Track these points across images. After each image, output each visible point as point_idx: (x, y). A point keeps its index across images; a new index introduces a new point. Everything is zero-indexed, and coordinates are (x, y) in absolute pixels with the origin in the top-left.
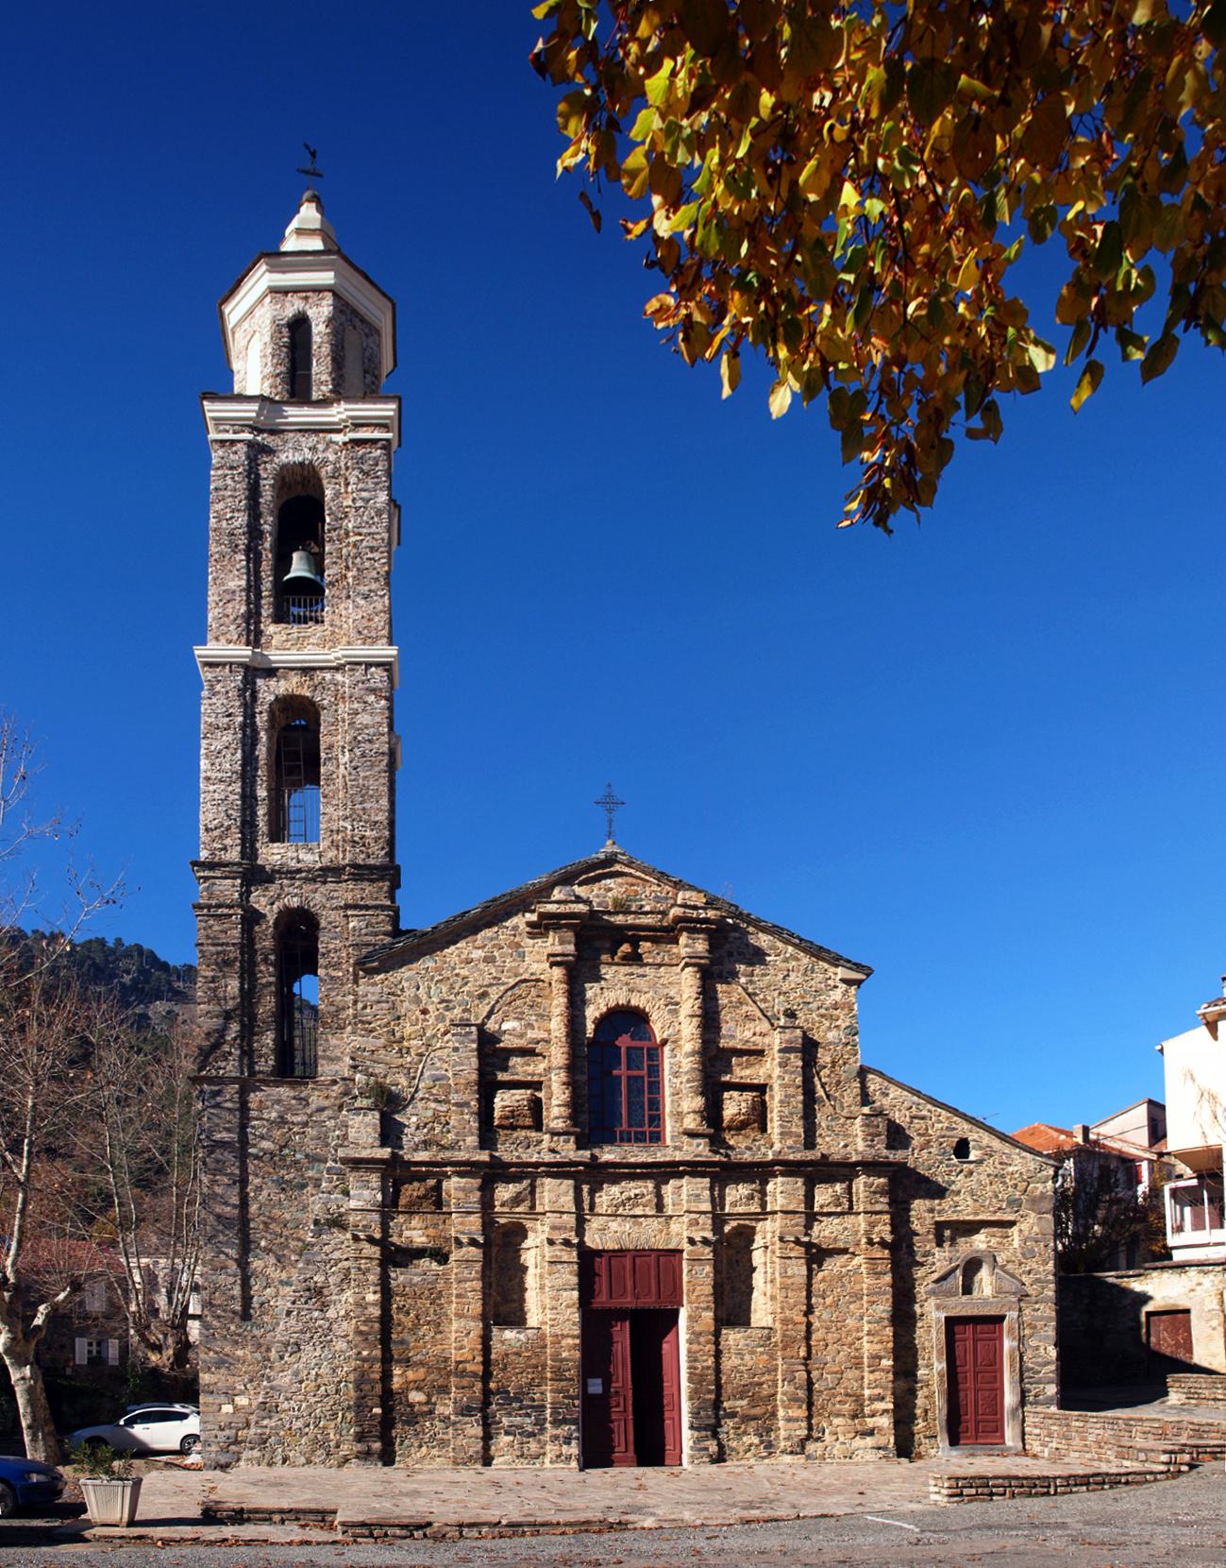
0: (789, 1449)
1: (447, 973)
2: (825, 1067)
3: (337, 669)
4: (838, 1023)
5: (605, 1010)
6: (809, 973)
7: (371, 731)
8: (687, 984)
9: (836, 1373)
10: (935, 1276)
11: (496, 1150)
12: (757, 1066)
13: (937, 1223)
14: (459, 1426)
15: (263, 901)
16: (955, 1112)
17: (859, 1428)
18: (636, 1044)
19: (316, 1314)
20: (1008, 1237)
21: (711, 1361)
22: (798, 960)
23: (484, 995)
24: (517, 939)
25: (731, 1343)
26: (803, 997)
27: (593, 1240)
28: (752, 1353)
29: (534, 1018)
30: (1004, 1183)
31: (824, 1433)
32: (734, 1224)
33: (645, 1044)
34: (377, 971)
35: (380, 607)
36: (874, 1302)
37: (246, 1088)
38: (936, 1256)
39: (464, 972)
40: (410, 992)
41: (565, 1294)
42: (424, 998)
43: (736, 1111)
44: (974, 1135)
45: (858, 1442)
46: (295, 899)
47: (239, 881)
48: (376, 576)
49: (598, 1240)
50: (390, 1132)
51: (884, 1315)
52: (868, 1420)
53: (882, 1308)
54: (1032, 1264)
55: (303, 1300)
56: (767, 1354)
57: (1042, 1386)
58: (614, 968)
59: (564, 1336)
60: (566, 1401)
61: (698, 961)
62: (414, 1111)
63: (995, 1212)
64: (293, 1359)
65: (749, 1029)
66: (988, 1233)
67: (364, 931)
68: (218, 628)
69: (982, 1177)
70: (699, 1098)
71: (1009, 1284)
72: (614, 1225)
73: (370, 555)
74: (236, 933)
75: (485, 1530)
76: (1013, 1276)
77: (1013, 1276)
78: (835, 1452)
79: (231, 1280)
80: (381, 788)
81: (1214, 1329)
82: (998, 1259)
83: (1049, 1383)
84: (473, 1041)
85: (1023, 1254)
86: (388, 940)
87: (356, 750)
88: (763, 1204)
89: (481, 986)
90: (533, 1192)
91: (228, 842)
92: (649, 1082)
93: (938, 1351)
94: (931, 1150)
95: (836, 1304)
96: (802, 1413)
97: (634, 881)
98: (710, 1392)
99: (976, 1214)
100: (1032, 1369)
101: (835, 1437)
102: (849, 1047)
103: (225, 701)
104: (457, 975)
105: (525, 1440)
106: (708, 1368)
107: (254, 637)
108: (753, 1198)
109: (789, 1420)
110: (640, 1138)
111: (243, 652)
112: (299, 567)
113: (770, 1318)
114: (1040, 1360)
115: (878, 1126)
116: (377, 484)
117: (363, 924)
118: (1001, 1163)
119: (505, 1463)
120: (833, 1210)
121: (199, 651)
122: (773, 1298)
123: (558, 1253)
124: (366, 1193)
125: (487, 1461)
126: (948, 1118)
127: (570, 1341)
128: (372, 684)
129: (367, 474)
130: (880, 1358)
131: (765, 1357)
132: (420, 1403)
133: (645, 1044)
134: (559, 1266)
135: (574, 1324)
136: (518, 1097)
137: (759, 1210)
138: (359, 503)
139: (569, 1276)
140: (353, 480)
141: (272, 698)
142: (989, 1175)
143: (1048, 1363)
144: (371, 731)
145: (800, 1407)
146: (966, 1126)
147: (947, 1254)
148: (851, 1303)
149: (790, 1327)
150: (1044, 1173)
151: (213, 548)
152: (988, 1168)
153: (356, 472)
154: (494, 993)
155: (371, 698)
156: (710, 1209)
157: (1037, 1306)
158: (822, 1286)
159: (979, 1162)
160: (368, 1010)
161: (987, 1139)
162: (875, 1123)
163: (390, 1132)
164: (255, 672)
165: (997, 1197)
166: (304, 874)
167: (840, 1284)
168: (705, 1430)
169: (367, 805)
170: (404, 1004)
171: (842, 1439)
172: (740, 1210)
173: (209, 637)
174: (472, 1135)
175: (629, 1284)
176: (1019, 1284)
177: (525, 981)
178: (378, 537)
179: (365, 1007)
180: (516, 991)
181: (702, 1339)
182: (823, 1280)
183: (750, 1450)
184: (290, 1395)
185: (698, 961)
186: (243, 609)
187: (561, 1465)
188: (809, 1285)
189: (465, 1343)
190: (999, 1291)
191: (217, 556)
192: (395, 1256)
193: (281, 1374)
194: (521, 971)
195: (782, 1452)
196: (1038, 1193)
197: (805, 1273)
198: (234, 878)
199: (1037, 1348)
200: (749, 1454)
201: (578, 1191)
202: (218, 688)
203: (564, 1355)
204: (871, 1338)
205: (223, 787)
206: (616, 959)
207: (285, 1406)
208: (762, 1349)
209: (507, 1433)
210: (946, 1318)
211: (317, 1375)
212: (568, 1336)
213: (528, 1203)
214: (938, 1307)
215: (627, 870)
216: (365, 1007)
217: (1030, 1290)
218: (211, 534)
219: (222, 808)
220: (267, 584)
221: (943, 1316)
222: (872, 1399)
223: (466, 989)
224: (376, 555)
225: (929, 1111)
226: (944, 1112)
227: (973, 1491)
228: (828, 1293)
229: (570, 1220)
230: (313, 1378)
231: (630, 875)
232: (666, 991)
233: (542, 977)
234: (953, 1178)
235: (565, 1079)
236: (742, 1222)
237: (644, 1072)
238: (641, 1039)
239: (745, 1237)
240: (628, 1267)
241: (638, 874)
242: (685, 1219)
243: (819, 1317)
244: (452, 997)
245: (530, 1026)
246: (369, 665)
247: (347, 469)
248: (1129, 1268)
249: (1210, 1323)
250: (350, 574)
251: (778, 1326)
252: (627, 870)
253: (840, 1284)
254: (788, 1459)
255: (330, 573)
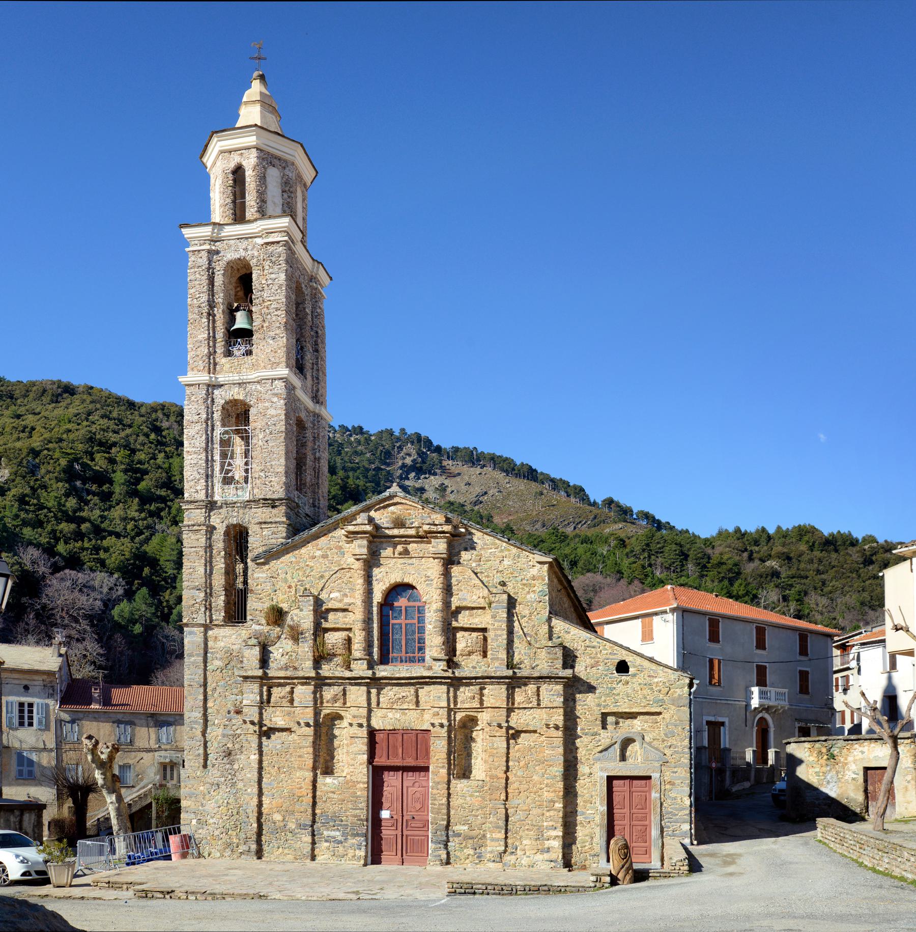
0: (493, 859)
1: (302, 565)
2: (525, 616)
3: (258, 382)
4: (534, 589)
5: (388, 585)
6: (516, 558)
7: (275, 419)
8: (434, 569)
9: (526, 810)
10: (600, 748)
11: (321, 668)
12: (483, 616)
13: (602, 713)
14: (298, 836)
15: (218, 521)
16: (615, 644)
17: (540, 847)
18: (411, 604)
19: (228, 766)
20: (657, 723)
21: (444, 801)
22: (509, 550)
23: (322, 577)
24: (341, 544)
25: (458, 789)
26: (512, 574)
27: (376, 723)
28: (471, 796)
29: (348, 590)
30: (652, 689)
31: (516, 850)
32: (463, 714)
33: (417, 604)
34: (264, 564)
35: (281, 344)
36: (551, 765)
37: (207, 628)
38: (602, 735)
39: (311, 564)
40: (282, 576)
41: (359, 757)
42: (290, 579)
43: (465, 645)
44: (630, 659)
45: (539, 857)
46: (235, 519)
47: (204, 510)
48: (278, 325)
49: (381, 724)
50: (264, 662)
51: (557, 774)
52: (546, 842)
53: (556, 769)
54: (672, 741)
55: (221, 758)
56: (481, 797)
57: (679, 824)
58: (394, 560)
59: (358, 783)
60: (359, 822)
61: (439, 555)
62: (281, 646)
63: (645, 706)
64: (215, 794)
65: (476, 595)
66: (642, 720)
67: (270, 537)
68: (193, 364)
69: (635, 686)
70: (440, 637)
71: (654, 754)
72: (390, 715)
73: (276, 313)
74: (203, 540)
75: (198, 896)
76: (657, 749)
77: (657, 749)
78: (523, 862)
79: (199, 743)
80: (281, 452)
81: (909, 782)
82: (646, 737)
83: (684, 822)
84: (311, 605)
85: (666, 735)
86: (284, 540)
87: (267, 431)
88: (481, 702)
89: (320, 572)
90: (344, 694)
91: (199, 488)
92: (418, 627)
93: (601, 799)
94: (600, 667)
95: (527, 765)
96: (502, 835)
97: (409, 507)
98: (443, 820)
99: (630, 708)
100: (671, 812)
101: (524, 852)
102: (541, 603)
103: (196, 406)
104: (307, 565)
105: (336, 845)
106: (442, 804)
107: (212, 366)
108: (474, 699)
109: (493, 840)
110: (411, 660)
111: (204, 378)
112: (241, 322)
113: (484, 774)
114: (677, 806)
115: (556, 654)
116: (280, 269)
117: (270, 533)
118: (649, 676)
119: (325, 859)
120: (527, 706)
121: (182, 379)
122: (486, 762)
123: (356, 732)
124: (251, 695)
125: (313, 858)
126: (611, 647)
127: (362, 786)
128: (276, 391)
129: (274, 263)
130: (554, 802)
131: (480, 799)
132: (279, 821)
133: (417, 604)
134: (356, 740)
135: (364, 775)
136: (336, 637)
137: (479, 706)
138: (270, 282)
139: (362, 746)
140: (267, 267)
141: (223, 402)
142: (640, 684)
143: (684, 809)
144: (275, 419)
145: (500, 832)
146: (624, 652)
147: (609, 734)
148: (536, 765)
149: (495, 780)
150: (682, 682)
151: (191, 316)
152: (640, 679)
153: (268, 262)
154: (327, 575)
155: (275, 399)
156: (446, 706)
157: (676, 770)
158: (518, 755)
159: (634, 675)
160: (259, 587)
161: (639, 660)
162: (554, 651)
163: (264, 662)
164: (212, 387)
165: (645, 698)
166: (239, 505)
167: (530, 753)
168: (440, 843)
169: (273, 463)
170: (279, 583)
171: (528, 854)
172: (467, 706)
173: (189, 369)
174: (309, 660)
175: (400, 751)
176: (662, 755)
177: (343, 569)
178: (280, 301)
179: (257, 585)
180: (338, 575)
181: (439, 787)
182: (518, 751)
183: (468, 858)
184: (213, 815)
185: (439, 555)
186: (206, 351)
187: (354, 862)
188: (508, 753)
189: (303, 785)
190: (646, 759)
191: (192, 321)
192: (266, 732)
193: (209, 802)
194: (342, 563)
195: (488, 860)
196: (676, 695)
197: (506, 746)
198: (201, 509)
199: (675, 798)
200: (467, 861)
201: (369, 693)
202: (193, 398)
203: (359, 793)
204: (549, 789)
205: (195, 456)
206: (396, 555)
207: (211, 821)
208: (478, 794)
209: (326, 841)
210: (608, 777)
211: (227, 803)
212: (360, 782)
213: (341, 701)
214: (601, 769)
215: (404, 501)
216: (257, 585)
217: (668, 758)
218: (189, 307)
219: (195, 469)
220: (220, 334)
221: (605, 775)
222: (548, 828)
223: (312, 573)
224: (279, 313)
225: (598, 642)
226: (608, 644)
227: (463, 891)
228: (522, 759)
229: (364, 712)
230: (225, 805)
231: (406, 504)
232: (426, 572)
233: (353, 567)
234: (614, 686)
235: (271, 655)
236: (468, 713)
237: (416, 621)
238: (414, 601)
239: (470, 723)
240: (400, 740)
241: (411, 503)
242: (431, 712)
243: (515, 775)
244: (304, 579)
245: (346, 595)
246: (273, 380)
247: (264, 260)
248: (819, 735)
249: (906, 778)
250: (265, 325)
251: (488, 779)
252: (404, 501)
253: (530, 753)
254: (491, 865)
255: (257, 323)
